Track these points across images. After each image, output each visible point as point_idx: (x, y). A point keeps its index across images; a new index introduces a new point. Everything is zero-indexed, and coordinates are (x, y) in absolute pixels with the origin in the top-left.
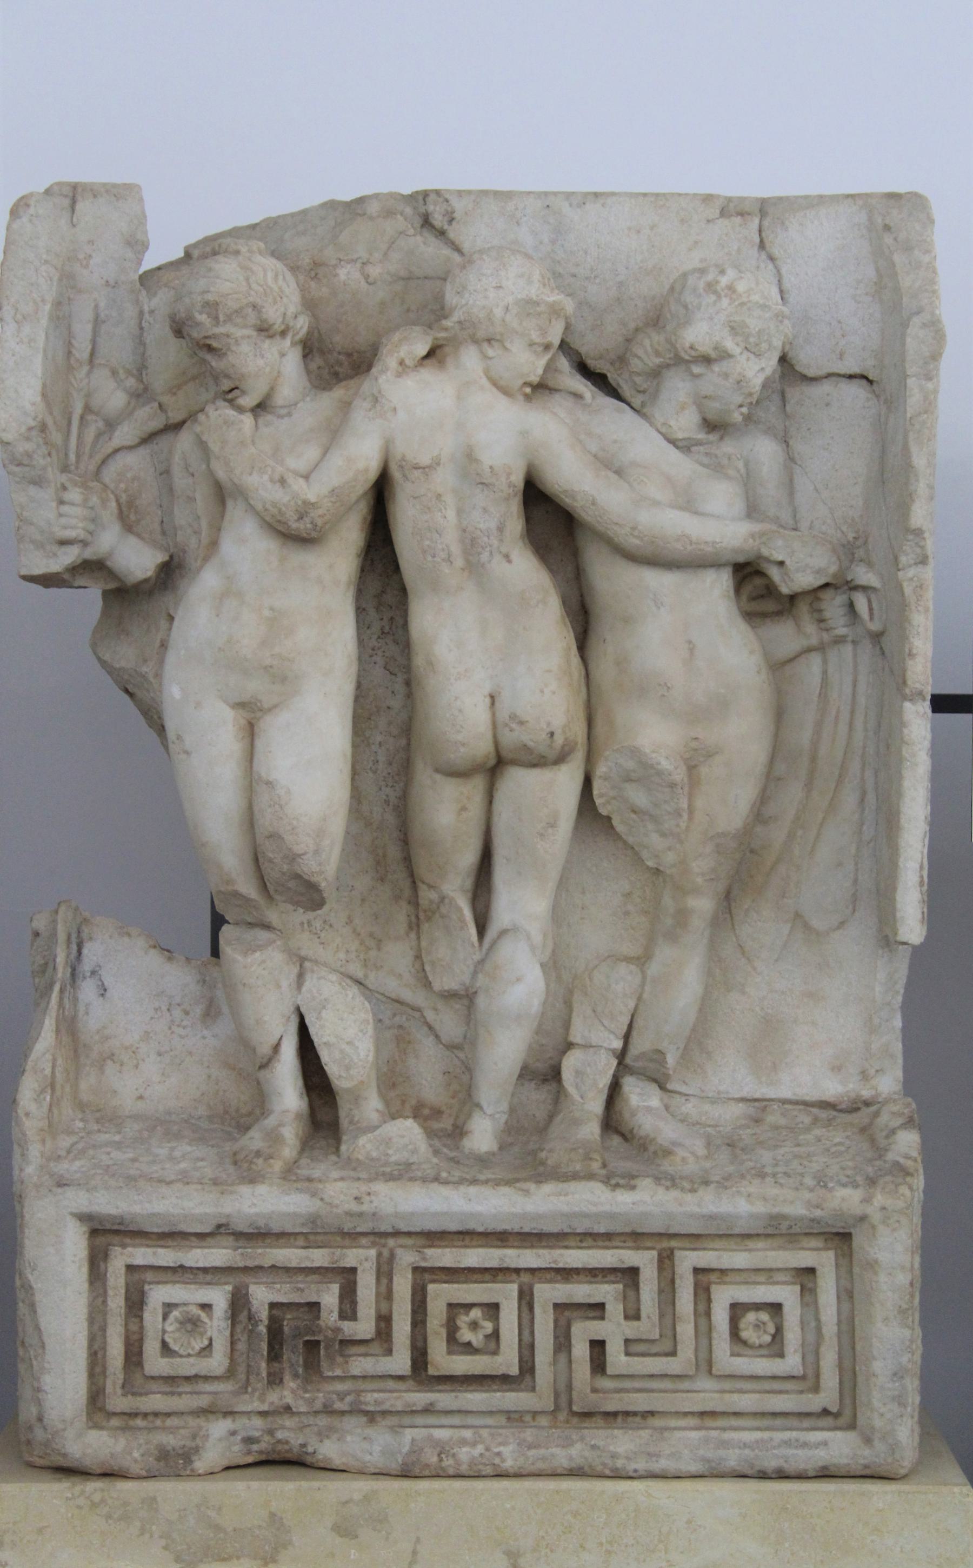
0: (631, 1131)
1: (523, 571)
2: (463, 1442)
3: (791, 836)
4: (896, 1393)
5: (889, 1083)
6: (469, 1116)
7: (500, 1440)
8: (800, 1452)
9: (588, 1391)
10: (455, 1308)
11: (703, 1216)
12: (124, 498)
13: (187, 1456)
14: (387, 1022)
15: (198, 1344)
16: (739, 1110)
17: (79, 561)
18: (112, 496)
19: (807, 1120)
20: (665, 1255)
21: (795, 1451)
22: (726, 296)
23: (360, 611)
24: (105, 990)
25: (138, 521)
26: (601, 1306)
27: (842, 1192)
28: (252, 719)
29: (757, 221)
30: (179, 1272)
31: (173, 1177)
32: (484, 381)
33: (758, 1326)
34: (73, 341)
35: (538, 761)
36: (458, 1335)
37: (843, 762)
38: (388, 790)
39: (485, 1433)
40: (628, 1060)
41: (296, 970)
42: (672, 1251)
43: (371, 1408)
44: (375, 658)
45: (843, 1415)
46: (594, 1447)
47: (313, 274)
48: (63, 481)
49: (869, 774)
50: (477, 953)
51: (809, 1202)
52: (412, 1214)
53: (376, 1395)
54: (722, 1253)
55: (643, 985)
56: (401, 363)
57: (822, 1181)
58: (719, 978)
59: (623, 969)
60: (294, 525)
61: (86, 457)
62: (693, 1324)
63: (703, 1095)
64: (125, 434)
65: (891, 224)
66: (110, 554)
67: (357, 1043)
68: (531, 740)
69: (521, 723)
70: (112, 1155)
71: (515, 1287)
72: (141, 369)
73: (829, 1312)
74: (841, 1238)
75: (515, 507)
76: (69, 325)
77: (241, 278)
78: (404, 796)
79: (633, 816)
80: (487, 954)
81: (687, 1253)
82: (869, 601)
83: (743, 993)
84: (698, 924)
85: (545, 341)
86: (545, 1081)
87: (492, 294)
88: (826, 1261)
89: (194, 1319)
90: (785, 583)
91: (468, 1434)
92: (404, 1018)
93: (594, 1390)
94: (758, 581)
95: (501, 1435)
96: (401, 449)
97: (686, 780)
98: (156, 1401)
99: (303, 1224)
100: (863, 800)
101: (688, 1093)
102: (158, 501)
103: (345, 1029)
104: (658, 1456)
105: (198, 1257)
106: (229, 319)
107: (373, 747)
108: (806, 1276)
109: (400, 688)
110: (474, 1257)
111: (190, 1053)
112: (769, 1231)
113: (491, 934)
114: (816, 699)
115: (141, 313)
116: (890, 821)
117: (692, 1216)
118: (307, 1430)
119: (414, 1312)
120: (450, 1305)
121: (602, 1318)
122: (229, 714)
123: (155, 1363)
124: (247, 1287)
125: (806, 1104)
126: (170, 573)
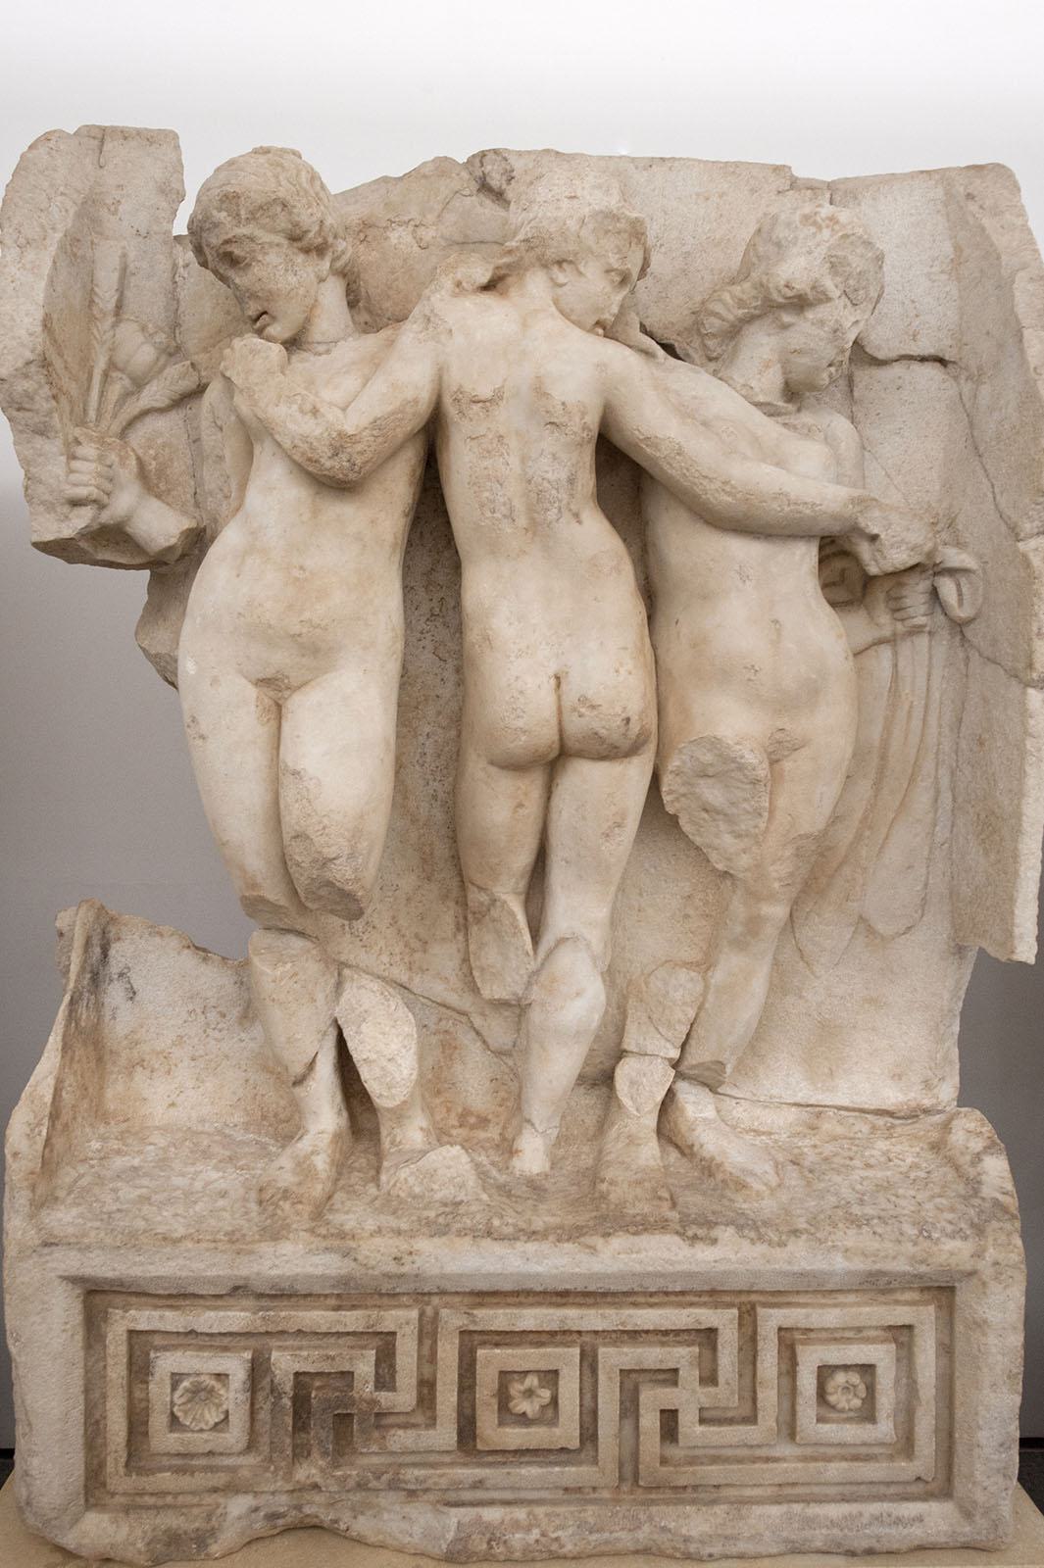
2: (516, 1525)
3: (859, 837)
4: (1003, 1465)
5: (948, 1091)
6: (519, 1132)
8: (893, 1531)
10: (505, 1377)
11: (795, 1274)
13: (202, 1539)
14: (433, 1027)
15: (212, 1417)
17: (96, 526)
19: (866, 1129)
21: (887, 1530)
22: (827, 227)
23: (407, 589)
24: (134, 993)
26: (702, 1421)
27: (950, 1245)
30: (191, 1338)
31: (181, 1231)
32: (553, 309)
33: (847, 1388)
34: (96, 289)
35: (609, 752)
36: (511, 1405)
39: (540, 1511)
40: (682, 1068)
42: (753, 1307)
43: (413, 1487)
44: (422, 643)
45: (943, 1485)
46: (664, 1529)
49: (944, 773)
50: (532, 963)
51: (913, 1257)
52: (461, 1275)
54: (809, 1310)
55: (704, 994)
56: (459, 284)
57: (924, 1230)
58: (780, 985)
59: (683, 975)
60: (328, 464)
61: (108, 416)
62: (776, 1391)
64: (155, 394)
66: (129, 518)
69: (593, 707)
70: (120, 1193)
71: (577, 1351)
72: (175, 326)
73: (927, 1374)
74: (942, 1291)
75: (586, 459)
76: (92, 275)
77: (269, 174)
78: (454, 791)
79: (705, 815)
80: (543, 964)
81: (771, 1311)
82: (958, 586)
83: (801, 997)
84: (770, 931)
85: (623, 267)
87: (565, 204)
88: (925, 1318)
90: (876, 561)
91: (520, 1514)
93: (664, 1461)
94: (838, 564)
96: (455, 378)
98: (165, 1480)
99: (333, 1286)
105: (210, 1320)
106: (253, 217)
107: (420, 738)
109: (450, 675)
110: (531, 1318)
111: (227, 1057)
113: (548, 940)
115: (175, 266)
116: (994, 829)
117: (786, 1274)
118: (340, 1505)
120: (503, 1373)
121: (675, 1383)
122: (252, 692)
123: (163, 1439)
125: (862, 1111)
126: (197, 542)
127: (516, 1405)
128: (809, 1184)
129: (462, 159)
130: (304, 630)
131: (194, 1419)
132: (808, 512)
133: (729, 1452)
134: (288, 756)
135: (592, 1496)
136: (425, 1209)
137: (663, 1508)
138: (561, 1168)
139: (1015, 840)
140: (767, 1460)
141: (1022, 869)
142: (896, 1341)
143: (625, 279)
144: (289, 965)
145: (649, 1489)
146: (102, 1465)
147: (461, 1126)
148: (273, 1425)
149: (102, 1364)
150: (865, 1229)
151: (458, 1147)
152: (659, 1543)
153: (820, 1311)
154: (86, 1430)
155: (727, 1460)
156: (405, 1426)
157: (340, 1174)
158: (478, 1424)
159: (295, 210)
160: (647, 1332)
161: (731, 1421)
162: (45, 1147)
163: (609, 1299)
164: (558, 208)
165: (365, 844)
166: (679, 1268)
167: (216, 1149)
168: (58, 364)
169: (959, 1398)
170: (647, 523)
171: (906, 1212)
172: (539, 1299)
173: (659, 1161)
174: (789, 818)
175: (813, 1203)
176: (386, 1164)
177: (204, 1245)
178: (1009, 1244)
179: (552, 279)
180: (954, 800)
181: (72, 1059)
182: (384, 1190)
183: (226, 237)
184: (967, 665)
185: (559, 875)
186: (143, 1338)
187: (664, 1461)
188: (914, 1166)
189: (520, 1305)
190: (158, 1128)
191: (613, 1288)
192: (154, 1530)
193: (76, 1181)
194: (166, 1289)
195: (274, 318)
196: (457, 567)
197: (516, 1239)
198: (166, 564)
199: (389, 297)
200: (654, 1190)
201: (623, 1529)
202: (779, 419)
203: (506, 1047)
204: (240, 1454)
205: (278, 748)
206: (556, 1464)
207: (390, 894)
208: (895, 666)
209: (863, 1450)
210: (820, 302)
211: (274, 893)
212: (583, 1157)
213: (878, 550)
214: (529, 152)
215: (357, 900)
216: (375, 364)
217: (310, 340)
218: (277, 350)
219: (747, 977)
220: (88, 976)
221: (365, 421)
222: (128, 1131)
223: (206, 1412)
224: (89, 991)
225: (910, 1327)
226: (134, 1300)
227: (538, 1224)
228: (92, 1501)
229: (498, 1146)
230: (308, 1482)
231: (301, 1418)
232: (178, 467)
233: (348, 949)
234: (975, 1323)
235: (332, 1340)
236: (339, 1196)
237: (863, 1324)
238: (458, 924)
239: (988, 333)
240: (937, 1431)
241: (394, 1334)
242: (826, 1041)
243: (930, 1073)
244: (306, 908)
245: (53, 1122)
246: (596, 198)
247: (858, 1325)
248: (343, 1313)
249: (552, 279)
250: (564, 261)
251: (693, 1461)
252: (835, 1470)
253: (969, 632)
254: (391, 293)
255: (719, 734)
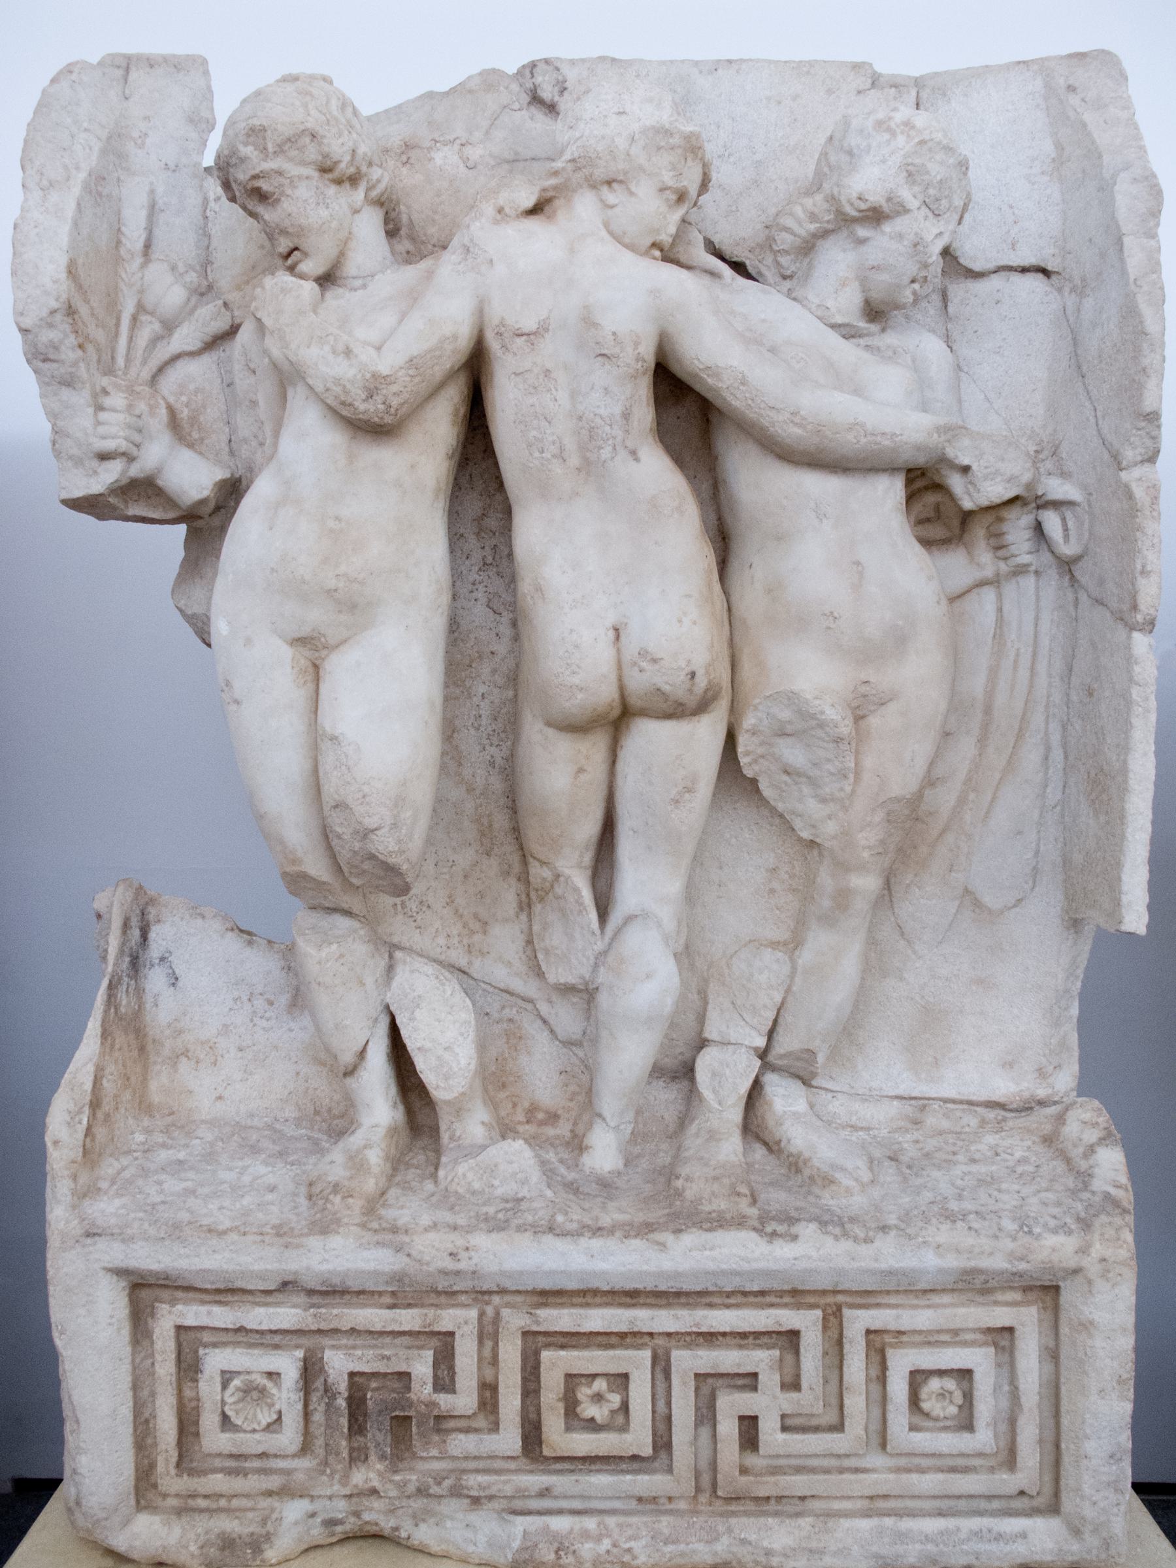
0: (779, 1142)
1: (655, 473)
2: (586, 1535)
3: (962, 801)
4: (1113, 1478)
5: (1065, 1080)
6: (590, 1126)
7: (630, 1532)
8: (993, 1547)
9: (737, 1473)
10: (572, 1380)
12: (184, 414)
13: (257, 1544)
14: (496, 1015)
15: (265, 1417)
16: (894, 1108)
17: (124, 481)
18: (162, 402)
19: (974, 1122)
20: (829, 1311)
21: (988, 1547)
22: (902, 133)
23: (455, 539)
24: (177, 979)
25: (202, 439)
26: (785, 1429)
27: (1051, 1240)
28: (313, 652)
29: (914, 93)
30: (241, 1335)
31: (227, 1224)
32: (604, 233)
33: (942, 1395)
34: (123, 229)
35: (675, 711)
36: (578, 1410)
37: (1024, 714)
38: (493, 750)
39: (611, 1521)
40: (771, 1058)
41: (383, 963)
42: (839, 1308)
43: (474, 1493)
44: (474, 595)
46: (744, 1542)
47: (404, 158)
48: (103, 384)
50: (599, 943)
52: (521, 1273)
53: (481, 1478)
54: (900, 1311)
56: (500, 210)
57: (1025, 1226)
58: (876, 964)
59: (768, 955)
60: (362, 407)
61: (137, 362)
62: (864, 1396)
63: (853, 1091)
64: (186, 337)
65: (1075, 91)
66: (159, 470)
67: (457, 1050)
68: (667, 683)
69: (654, 661)
70: (165, 1186)
71: (647, 1354)
72: (206, 264)
73: (1030, 1380)
74: (1046, 1291)
75: (644, 389)
76: (119, 212)
77: (298, 103)
78: (511, 757)
79: (785, 778)
80: (610, 944)
82: (1064, 520)
83: (901, 979)
84: (860, 905)
85: (679, 185)
86: (674, 1078)
88: (1028, 1320)
89: (258, 1391)
91: (590, 1523)
92: (515, 1010)
93: (744, 1471)
94: (931, 498)
95: (630, 1525)
96: (497, 311)
97: (854, 733)
98: (217, 1482)
100: (1046, 758)
101: (834, 1089)
102: (225, 416)
103: (442, 1032)
104: (821, 1552)
105: (260, 1317)
106: (280, 151)
107: (475, 699)
108: (1002, 1338)
109: (506, 631)
110: (597, 1319)
111: (276, 1048)
112: (960, 1286)
113: (615, 919)
114: (990, 640)
115: (206, 201)
117: (873, 1272)
118: (400, 1512)
119: (525, 1380)
120: (569, 1377)
121: (754, 1388)
122: (287, 653)
123: (214, 1439)
124: (323, 1349)
125: (971, 1103)
126: (231, 492)
127: (584, 1410)
128: (905, 1180)
129: (512, 69)
130: (341, 585)
131: (246, 1418)
132: (887, 443)
133: (815, 1462)
134: (327, 722)
135: (669, 1507)
136: (484, 1204)
137: (744, 1520)
138: (637, 1166)
139: (1122, 800)
140: (857, 1470)
141: (1129, 830)
142: (995, 1345)
143: (681, 197)
144: (334, 947)
145: (729, 1500)
146: (152, 1466)
147: (528, 1122)
148: (328, 1426)
149: (149, 1361)
150: (959, 1224)
151: (521, 1142)
152: (739, 1556)
153: (912, 1312)
154: (135, 1430)
155: (813, 1470)
156: (467, 1431)
157: (395, 1169)
158: (544, 1429)
159: (325, 141)
160: (724, 1334)
161: (816, 1429)
162: (86, 1135)
163: (683, 1300)
164: (606, 125)
165: (409, 814)
166: (755, 1266)
167: (266, 1144)
168: (84, 310)
169: (1065, 1405)
170: (716, 458)
171: (1007, 1207)
172: (609, 1299)
173: (741, 1157)
174: (878, 779)
175: (907, 1200)
176: (444, 1159)
177: (251, 1238)
178: (1119, 1239)
179: (601, 200)
180: (1066, 757)
181: (112, 1046)
182: (442, 1187)
183: (253, 172)
184: (1076, 606)
185: (627, 847)
186: (192, 1335)
187: (744, 1471)
188: (1023, 1161)
189: (588, 1305)
190: (203, 1122)
191: (686, 1287)
192: (207, 1533)
193: (119, 1173)
194: (213, 1283)
195: (306, 254)
196: (508, 512)
197: (582, 1235)
198: (201, 518)
199: (433, 221)
200: (733, 1186)
201: (700, 1541)
202: (862, 341)
203: (574, 1037)
204: (294, 1456)
205: (316, 711)
206: (628, 1472)
207: (445, 870)
208: (1000, 610)
209: (961, 1462)
210: (898, 214)
211: (316, 867)
212: (662, 1154)
213: (971, 483)
214: (583, 61)
215: (401, 874)
216: (412, 298)
217: (344, 275)
218: (309, 288)
219: (838, 955)
220: (127, 959)
221: (400, 359)
222: (174, 1125)
223: (258, 1411)
224: (128, 976)
225: (1010, 1330)
226: (180, 1294)
227: (606, 1220)
228: (143, 1502)
229: (568, 1143)
230: (366, 1486)
231: (357, 1420)
232: (212, 414)
233: (400, 930)
234: (1081, 1324)
235: (388, 1340)
236: (393, 1192)
237: (958, 1326)
238: (521, 902)
239: (1090, 240)
240: (1041, 1441)
241: (452, 1334)
242: (930, 1028)
243: (1044, 1060)
244: (351, 885)
245: (94, 1110)
246: (647, 110)
247: (952, 1326)
248: (398, 1311)
249: (601, 200)
250: (614, 181)
251: (775, 1471)
252: (929, 1482)
253: (1078, 570)
254: (437, 217)
255: (795, 688)
